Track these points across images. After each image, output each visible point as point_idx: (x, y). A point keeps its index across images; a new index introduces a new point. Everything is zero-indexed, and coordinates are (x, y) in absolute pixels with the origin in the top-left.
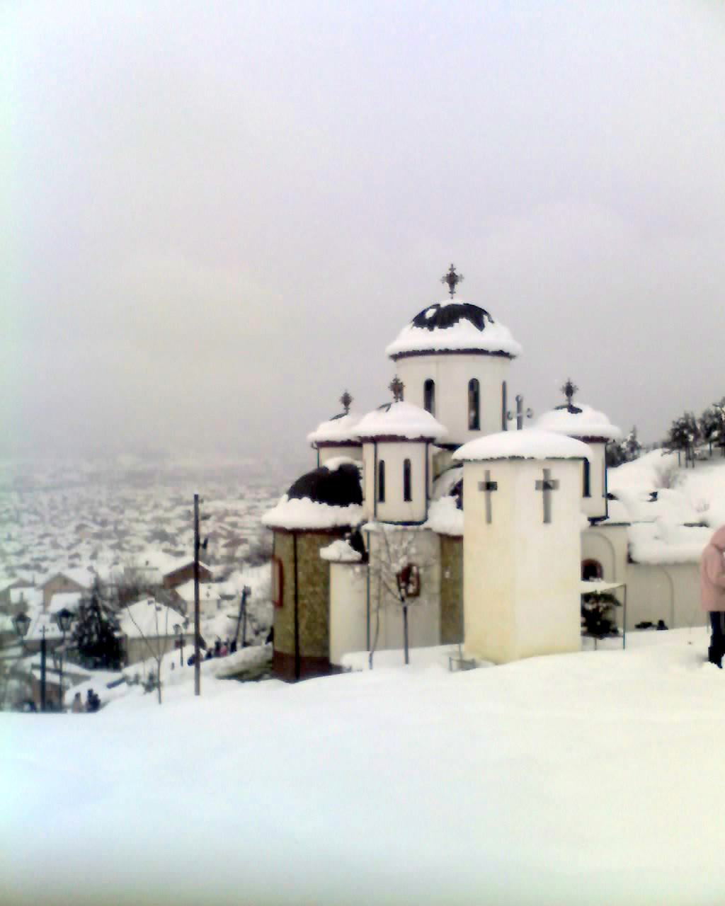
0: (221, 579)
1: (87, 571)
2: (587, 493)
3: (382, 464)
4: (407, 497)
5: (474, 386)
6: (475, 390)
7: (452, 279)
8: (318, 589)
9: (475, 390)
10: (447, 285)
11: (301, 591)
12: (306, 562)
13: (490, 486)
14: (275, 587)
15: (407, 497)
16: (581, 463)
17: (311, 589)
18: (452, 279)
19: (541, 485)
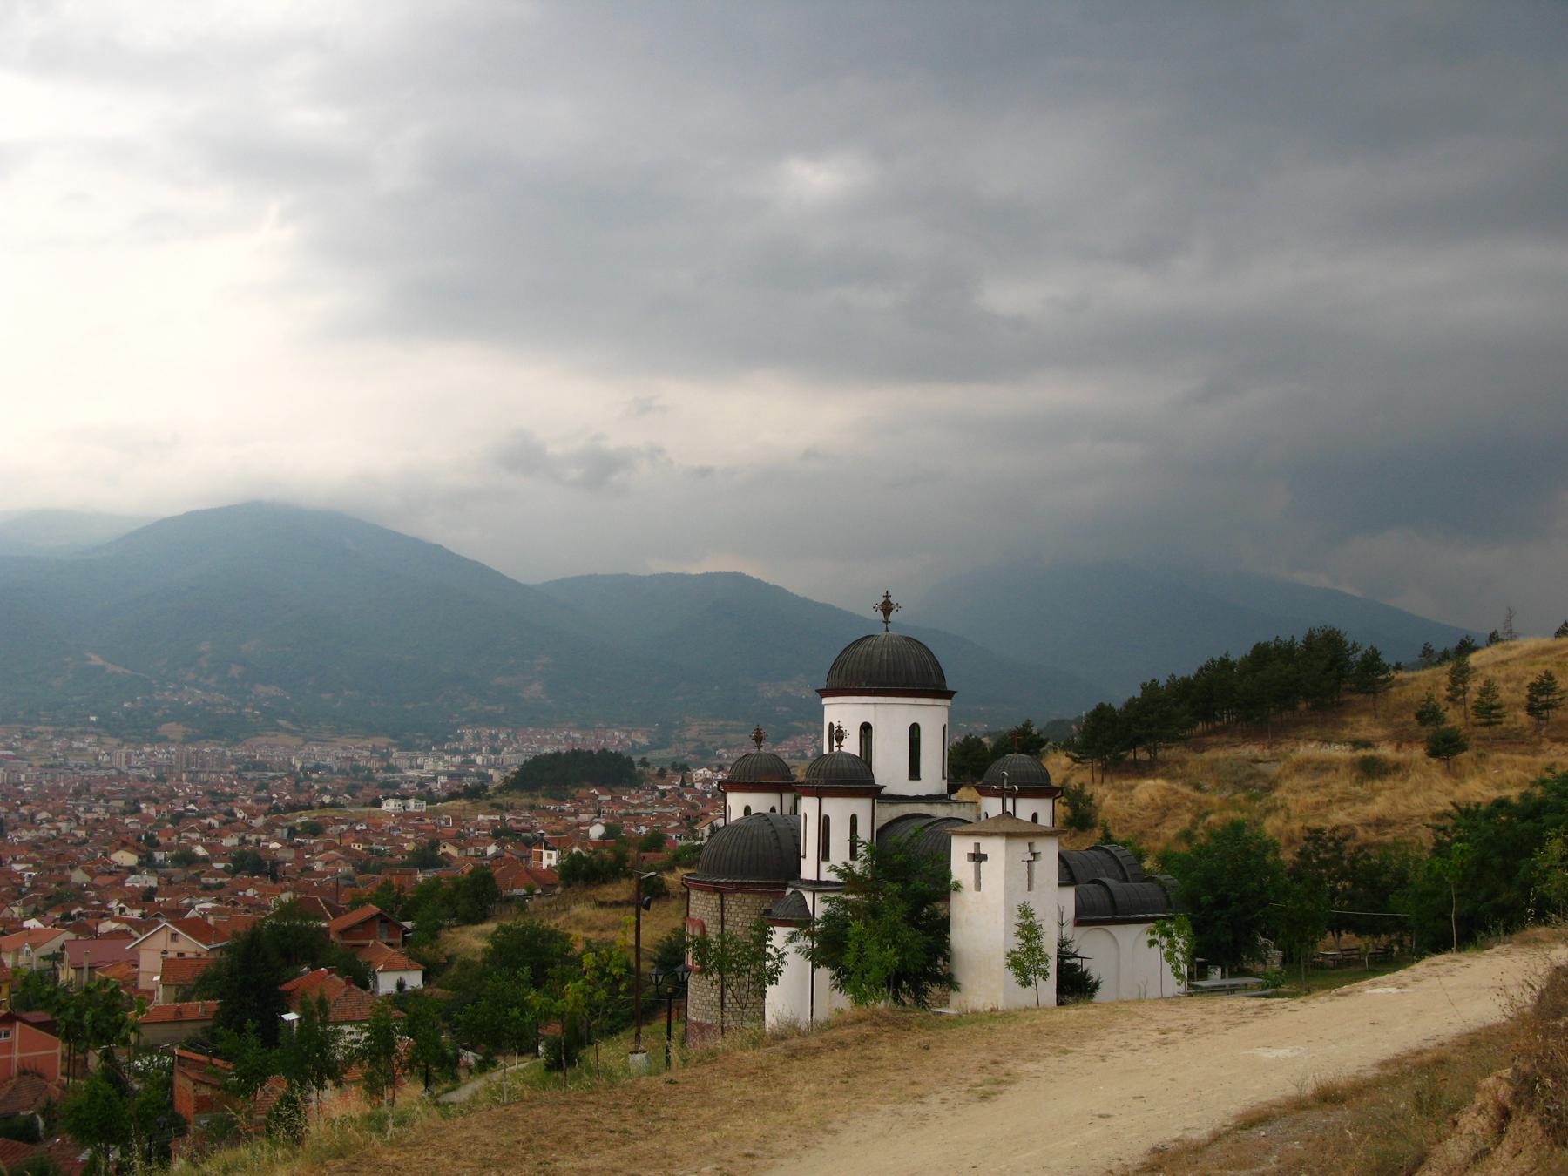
3: (827, 819)
7: (887, 608)
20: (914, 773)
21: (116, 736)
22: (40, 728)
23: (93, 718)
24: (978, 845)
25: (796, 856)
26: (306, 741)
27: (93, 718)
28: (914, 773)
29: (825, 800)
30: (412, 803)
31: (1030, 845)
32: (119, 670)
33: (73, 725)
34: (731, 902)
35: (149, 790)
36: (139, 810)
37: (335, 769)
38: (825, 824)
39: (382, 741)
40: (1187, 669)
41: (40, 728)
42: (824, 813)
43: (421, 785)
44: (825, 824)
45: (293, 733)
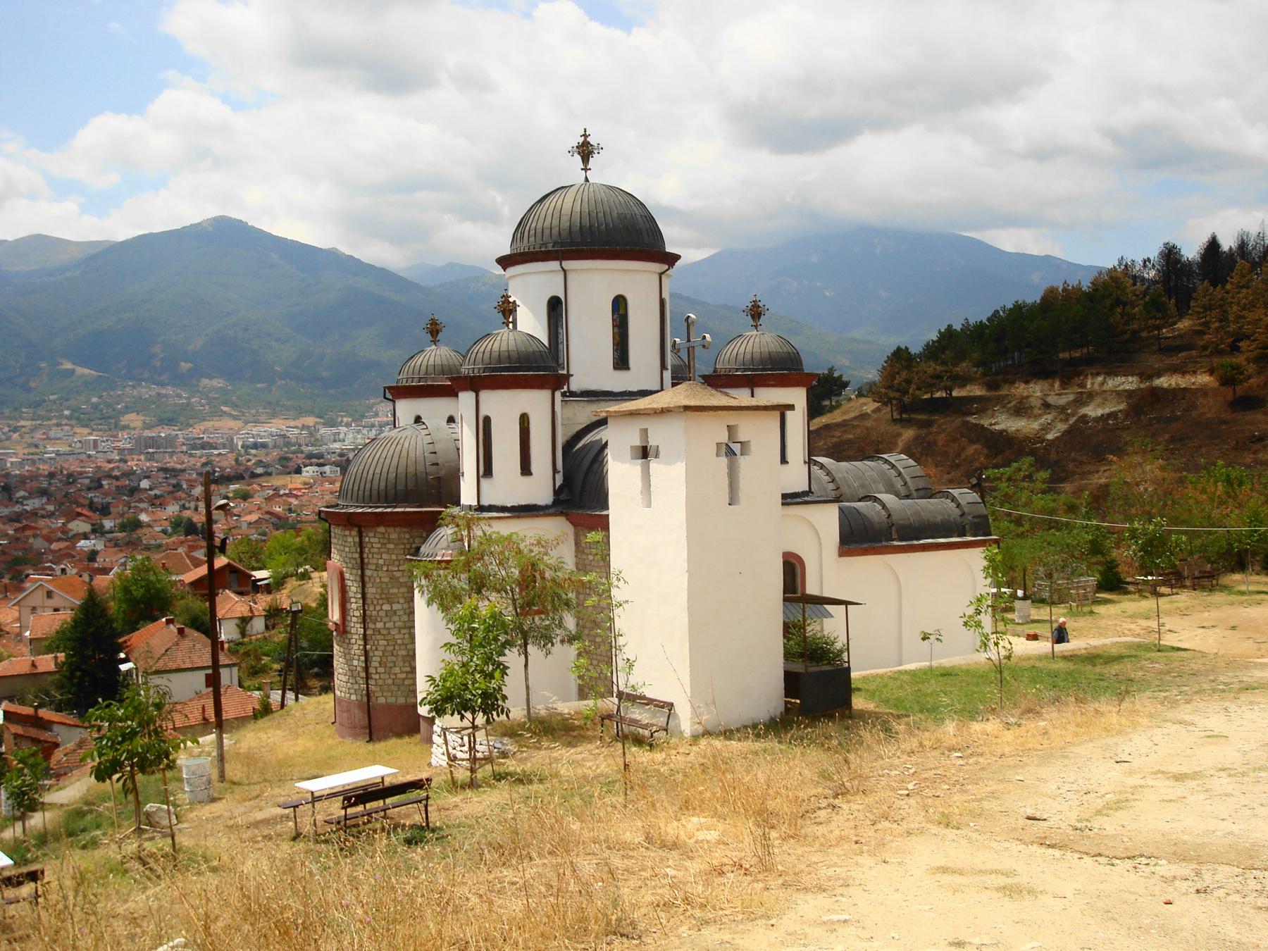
0: (268, 589)
1: (629, 450)
2: (784, 460)
3: (487, 420)
4: (526, 469)
5: (619, 305)
6: (622, 312)
7: (585, 151)
8: (371, 626)
9: (622, 312)
10: (578, 158)
11: (371, 611)
12: (378, 568)
13: (644, 453)
14: (500, 518)
15: (526, 469)
16: (777, 413)
17: (386, 607)
18: (585, 151)
19: (652, 453)
20: (622, 361)
21: (87, 426)
22: (23, 423)
23: (67, 413)
24: (645, 432)
25: (454, 475)
26: (246, 423)
27: (67, 413)
28: (622, 361)
29: (485, 395)
30: (327, 469)
31: (730, 429)
32: (87, 371)
33: (50, 419)
34: (372, 539)
35: (112, 469)
36: (101, 486)
37: (271, 445)
38: (485, 429)
39: (310, 421)
40: (980, 313)
41: (23, 423)
42: (482, 413)
43: (341, 455)
44: (485, 429)
45: (235, 418)
